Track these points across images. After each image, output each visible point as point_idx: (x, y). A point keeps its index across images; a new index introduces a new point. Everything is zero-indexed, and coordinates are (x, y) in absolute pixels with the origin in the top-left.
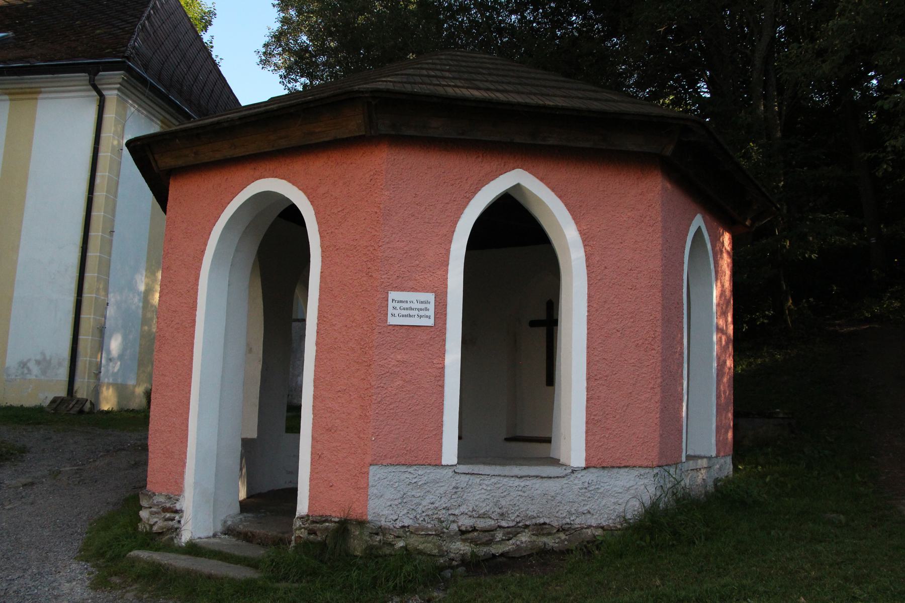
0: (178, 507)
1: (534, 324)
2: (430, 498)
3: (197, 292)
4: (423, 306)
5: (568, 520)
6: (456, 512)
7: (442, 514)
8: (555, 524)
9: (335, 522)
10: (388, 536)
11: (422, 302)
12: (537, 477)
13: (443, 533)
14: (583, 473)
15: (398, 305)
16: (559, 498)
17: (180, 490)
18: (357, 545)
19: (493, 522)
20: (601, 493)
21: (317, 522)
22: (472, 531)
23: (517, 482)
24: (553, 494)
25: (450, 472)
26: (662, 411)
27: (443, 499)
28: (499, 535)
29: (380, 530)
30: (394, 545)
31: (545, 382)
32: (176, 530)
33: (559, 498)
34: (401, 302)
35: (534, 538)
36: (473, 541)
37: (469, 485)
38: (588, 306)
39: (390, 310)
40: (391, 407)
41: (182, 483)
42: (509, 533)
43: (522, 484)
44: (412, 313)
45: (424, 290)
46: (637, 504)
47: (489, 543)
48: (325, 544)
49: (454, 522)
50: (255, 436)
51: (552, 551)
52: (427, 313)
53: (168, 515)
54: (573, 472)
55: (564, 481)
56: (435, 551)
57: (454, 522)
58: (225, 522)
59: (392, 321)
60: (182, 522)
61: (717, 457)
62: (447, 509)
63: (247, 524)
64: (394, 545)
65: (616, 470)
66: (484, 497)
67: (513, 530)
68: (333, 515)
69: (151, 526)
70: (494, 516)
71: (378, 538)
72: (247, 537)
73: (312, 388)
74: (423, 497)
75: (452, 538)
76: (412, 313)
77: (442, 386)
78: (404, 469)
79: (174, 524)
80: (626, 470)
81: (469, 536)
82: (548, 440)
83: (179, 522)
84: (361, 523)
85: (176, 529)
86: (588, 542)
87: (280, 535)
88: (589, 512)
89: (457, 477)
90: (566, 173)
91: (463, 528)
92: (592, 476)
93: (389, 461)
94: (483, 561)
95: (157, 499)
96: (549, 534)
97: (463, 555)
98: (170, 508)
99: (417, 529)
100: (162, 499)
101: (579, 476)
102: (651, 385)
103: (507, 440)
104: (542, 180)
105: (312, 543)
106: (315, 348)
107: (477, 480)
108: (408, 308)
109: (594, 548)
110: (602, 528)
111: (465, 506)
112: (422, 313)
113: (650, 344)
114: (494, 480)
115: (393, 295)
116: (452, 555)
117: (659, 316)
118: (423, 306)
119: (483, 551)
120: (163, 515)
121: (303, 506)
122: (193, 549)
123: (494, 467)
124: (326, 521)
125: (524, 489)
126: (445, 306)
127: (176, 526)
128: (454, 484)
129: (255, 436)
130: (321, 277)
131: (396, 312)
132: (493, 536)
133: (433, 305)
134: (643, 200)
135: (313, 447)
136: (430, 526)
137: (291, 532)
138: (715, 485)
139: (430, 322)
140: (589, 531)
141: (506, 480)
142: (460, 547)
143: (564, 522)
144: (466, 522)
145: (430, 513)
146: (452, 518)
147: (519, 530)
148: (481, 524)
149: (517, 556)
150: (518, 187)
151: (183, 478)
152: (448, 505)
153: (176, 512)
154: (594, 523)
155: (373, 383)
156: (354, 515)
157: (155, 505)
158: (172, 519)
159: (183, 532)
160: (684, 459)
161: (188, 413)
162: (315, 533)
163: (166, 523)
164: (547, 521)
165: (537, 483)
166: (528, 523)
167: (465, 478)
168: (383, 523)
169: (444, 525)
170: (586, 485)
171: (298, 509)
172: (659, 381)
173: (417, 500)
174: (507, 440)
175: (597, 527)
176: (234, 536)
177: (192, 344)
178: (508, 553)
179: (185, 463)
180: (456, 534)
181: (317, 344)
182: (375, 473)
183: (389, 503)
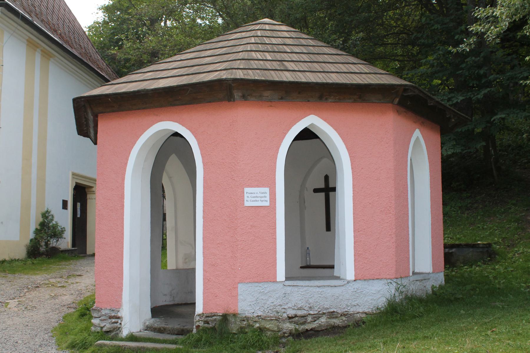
0: (119, 314)
1: (316, 191)
2: (271, 300)
3: (124, 188)
4: (263, 195)
5: (346, 310)
6: (286, 307)
7: (279, 309)
8: (339, 311)
9: (220, 316)
10: (250, 321)
11: (262, 193)
12: (328, 286)
13: (279, 318)
14: (354, 282)
15: (250, 195)
16: (341, 298)
17: (120, 305)
18: (234, 327)
19: (305, 312)
20: (364, 294)
21: (209, 317)
22: (295, 317)
24: (337, 295)
26: (396, 247)
27: (278, 300)
28: (309, 319)
29: (247, 319)
30: (253, 326)
31: (325, 229)
32: (119, 329)
33: (341, 298)
34: (251, 193)
35: (328, 320)
36: (296, 323)
38: (353, 191)
39: (246, 198)
40: (249, 251)
41: (121, 301)
42: (314, 317)
43: (321, 290)
44: (257, 199)
46: (384, 299)
47: (304, 323)
48: (215, 329)
49: (284, 312)
51: (338, 327)
52: (265, 199)
53: (113, 320)
55: (343, 288)
56: (276, 329)
57: (284, 312)
58: (145, 323)
59: (247, 204)
60: (123, 324)
61: (433, 273)
62: (281, 305)
63: (158, 323)
64: (253, 326)
65: (371, 281)
66: (300, 298)
67: (317, 315)
68: (218, 312)
69: (102, 328)
70: (306, 308)
71: (245, 323)
72: (160, 331)
73: (202, 242)
75: (284, 321)
76: (257, 199)
77: (275, 239)
78: (256, 284)
79: (118, 325)
80: (377, 281)
81: (293, 320)
82: (332, 267)
83: (121, 324)
84: (235, 315)
85: (119, 328)
86: (359, 321)
87: (182, 327)
88: (358, 305)
89: (285, 288)
91: (290, 316)
92: (359, 285)
93: (248, 281)
94: (302, 333)
95: (103, 312)
96: (336, 317)
97: (291, 330)
98: (114, 316)
99: (266, 317)
100: (107, 312)
101: (351, 285)
102: (390, 233)
103: (301, 267)
104: (325, 120)
105: (207, 328)
106: (202, 220)
107: (296, 289)
108: (255, 196)
109: (362, 324)
110: (366, 313)
111: (290, 304)
112: (262, 199)
113: (388, 210)
114: (305, 289)
115: (247, 190)
116: (285, 330)
118: (263, 195)
119: (301, 328)
120: (110, 321)
121: (199, 309)
122: (132, 338)
123: (305, 281)
124: (214, 316)
125: (322, 293)
126: (275, 194)
127: (119, 326)
128: (284, 292)
130: (204, 180)
131: (249, 199)
132: (306, 319)
133: (269, 196)
134: (383, 125)
135: (204, 275)
136: (272, 315)
137: (192, 323)
138: (432, 289)
139: (267, 204)
140: (358, 315)
141: (312, 288)
142: (288, 326)
143: (344, 310)
144: (291, 313)
145: (272, 308)
146: (283, 310)
147: (320, 316)
148: (300, 313)
149: (320, 329)
150: (312, 125)
151: (121, 298)
152: (281, 303)
153: (119, 318)
154: (361, 311)
155: (238, 239)
156: (231, 311)
157: (103, 315)
158: (117, 323)
159: (123, 330)
160: (411, 274)
161: (122, 260)
162: (208, 323)
163: (112, 325)
164: (335, 310)
165: (329, 291)
166: (324, 312)
167: (289, 289)
168: (247, 314)
169: (279, 314)
170: (356, 290)
171: (196, 310)
172: (394, 231)
173: (264, 301)
174: (301, 267)
175: (363, 313)
176: (151, 331)
177: (123, 219)
178: (314, 328)
179: (122, 289)
180: (286, 319)
181: (204, 218)
182: (242, 288)
183: (249, 304)
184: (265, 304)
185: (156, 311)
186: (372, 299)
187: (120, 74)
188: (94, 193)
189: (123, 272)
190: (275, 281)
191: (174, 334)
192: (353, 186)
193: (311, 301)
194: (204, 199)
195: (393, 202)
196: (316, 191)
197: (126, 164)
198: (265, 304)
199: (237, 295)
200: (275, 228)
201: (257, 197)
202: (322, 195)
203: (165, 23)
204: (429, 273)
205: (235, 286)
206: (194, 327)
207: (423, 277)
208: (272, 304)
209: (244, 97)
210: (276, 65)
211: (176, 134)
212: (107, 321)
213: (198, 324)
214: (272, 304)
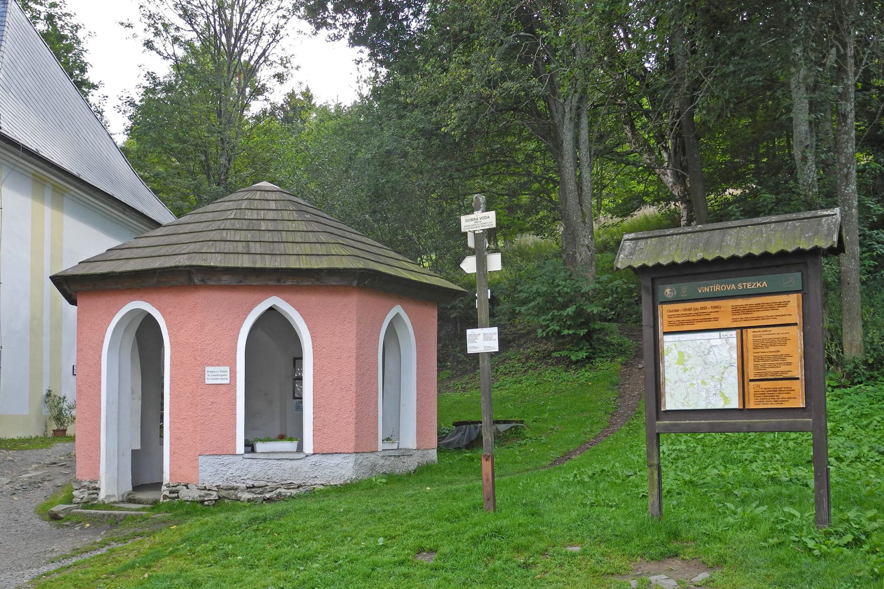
0: (97, 486)
2: (231, 471)
23: (276, 462)
25: (241, 458)
37: (251, 464)
39: (207, 377)
45: (224, 365)
50: (139, 448)
54: (307, 456)
59: (207, 382)
74: (227, 471)
90: (300, 297)
92: (317, 458)
107: (255, 461)
108: (216, 375)
115: (208, 369)
117: (354, 372)
129: (139, 448)
133: (230, 374)
139: (228, 382)
144: (250, 483)
165: (289, 464)
187: (231, 193)
193: (269, 472)
203: (482, 263)
213: (164, 493)
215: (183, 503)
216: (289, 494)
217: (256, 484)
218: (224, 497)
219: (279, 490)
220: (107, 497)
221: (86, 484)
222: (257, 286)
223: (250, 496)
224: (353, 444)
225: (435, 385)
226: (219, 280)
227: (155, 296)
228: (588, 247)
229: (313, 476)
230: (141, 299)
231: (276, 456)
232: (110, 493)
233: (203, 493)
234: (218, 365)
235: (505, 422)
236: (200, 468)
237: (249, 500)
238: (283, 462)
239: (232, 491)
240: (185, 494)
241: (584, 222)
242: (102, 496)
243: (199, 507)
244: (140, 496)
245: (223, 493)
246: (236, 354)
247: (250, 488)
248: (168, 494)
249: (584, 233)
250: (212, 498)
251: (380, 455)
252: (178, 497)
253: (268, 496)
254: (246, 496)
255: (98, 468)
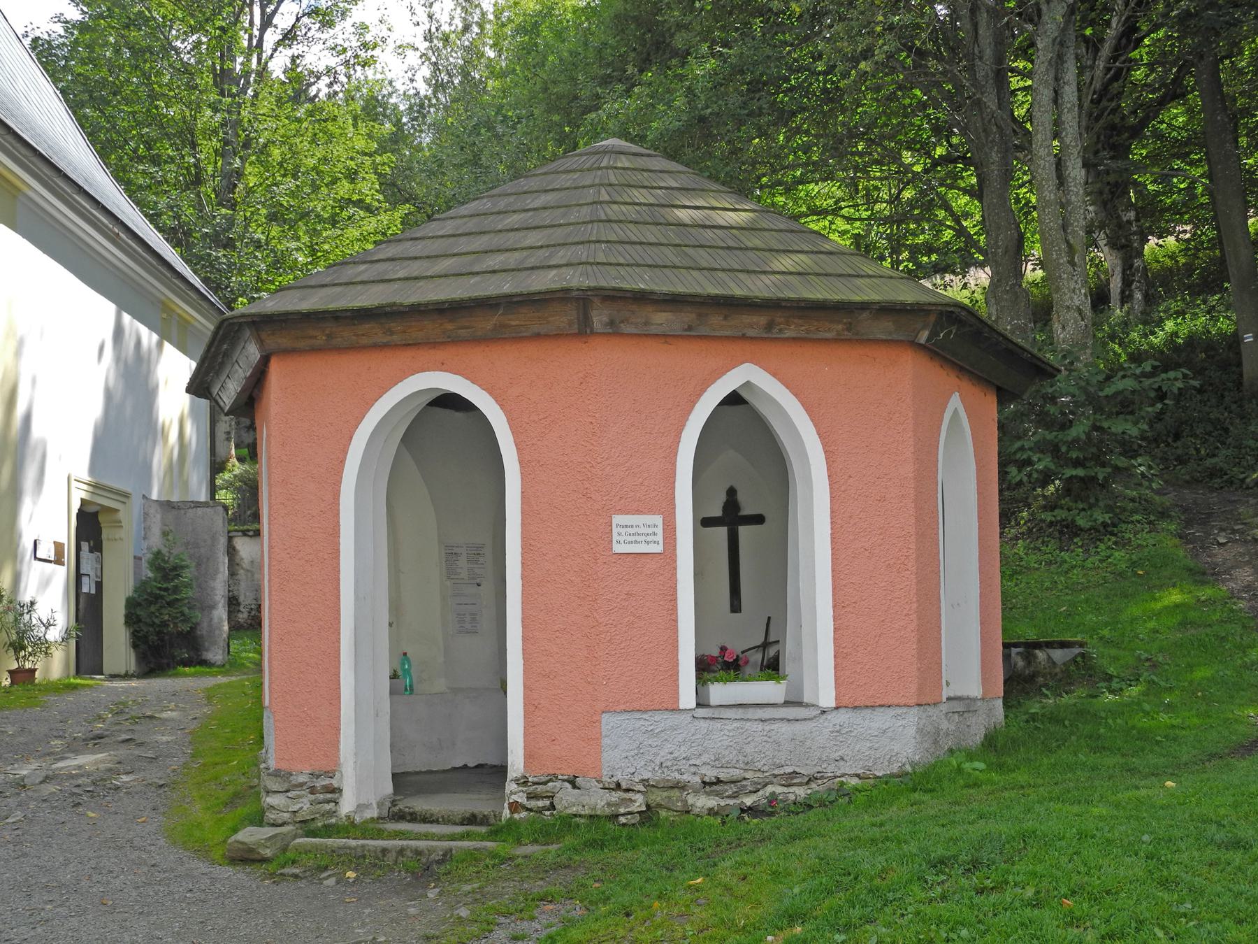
1: (758, 519)
2: (668, 747)
12: (782, 720)
15: (623, 531)
23: (760, 726)
27: (683, 748)
33: (808, 743)
39: (615, 537)
43: (767, 728)
45: (650, 511)
54: (824, 712)
55: (811, 724)
59: (617, 549)
74: (661, 747)
77: (676, 621)
78: (638, 715)
80: (882, 709)
88: (842, 759)
89: (696, 723)
91: (707, 779)
92: (843, 717)
93: (622, 707)
106: (520, 582)
107: (718, 725)
108: (634, 534)
110: (858, 776)
112: (649, 538)
114: (736, 724)
115: (618, 519)
118: (650, 530)
130: (523, 497)
131: (621, 539)
133: (664, 533)
135: (526, 697)
139: (659, 549)
144: (711, 774)
151: (338, 750)
165: (785, 728)
170: (838, 728)
172: (915, 605)
173: (654, 750)
183: (624, 755)
184: (656, 755)
185: (400, 780)
186: (870, 748)
188: (118, 524)
189: (339, 693)
190: (676, 710)
191: (455, 824)
192: (832, 512)
194: (523, 538)
195: (913, 546)
196: (758, 519)
197: (343, 462)
198: (656, 755)
199: (598, 739)
200: (676, 600)
201: (638, 534)
202: (722, 532)
204: (974, 700)
205: (595, 718)
206: (506, 805)
207: (964, 705)
208: (669, 756)
209: (614, 331)
210: (670, 256)
211: (449, 401)
212: (305, 800)
213: (514, 798)
214: (669, 756)
215: (568, 823)
216: (792, 797)
217: (722, 776)
218: (659, 806)
219: (770, 789)
220: (360, 807)
221: (301, 779)
222: (727, 337)
223: (713, 802)
224: (913, 688)
225: (998, 564)
226: (646, 323)
227: (476, 356)
228: (1080, 311)
229: (836, 755)
230: (442, 367)
231: (761, 713)
232: (363, 801)
233: (616, 796)
234: (638, 512)
235: (1063, 645)
236: (605, 741)
237: (711, 812)
238: (775, 726)
239: (676, 793)
240: (568, 800)
241: (1072, 263)
242: (347, 805)
243: (600, 831)
244: (420, 805)
245: (658, 797)
246: (673, 488)
247: (709, 785)
248: (521, 798)
249: (1072, 285)
250: (635, 807)
251: (944, 708)
252: (552, 807)
253: (748, 801)
254: (703, 802)
255: (336, 744)
